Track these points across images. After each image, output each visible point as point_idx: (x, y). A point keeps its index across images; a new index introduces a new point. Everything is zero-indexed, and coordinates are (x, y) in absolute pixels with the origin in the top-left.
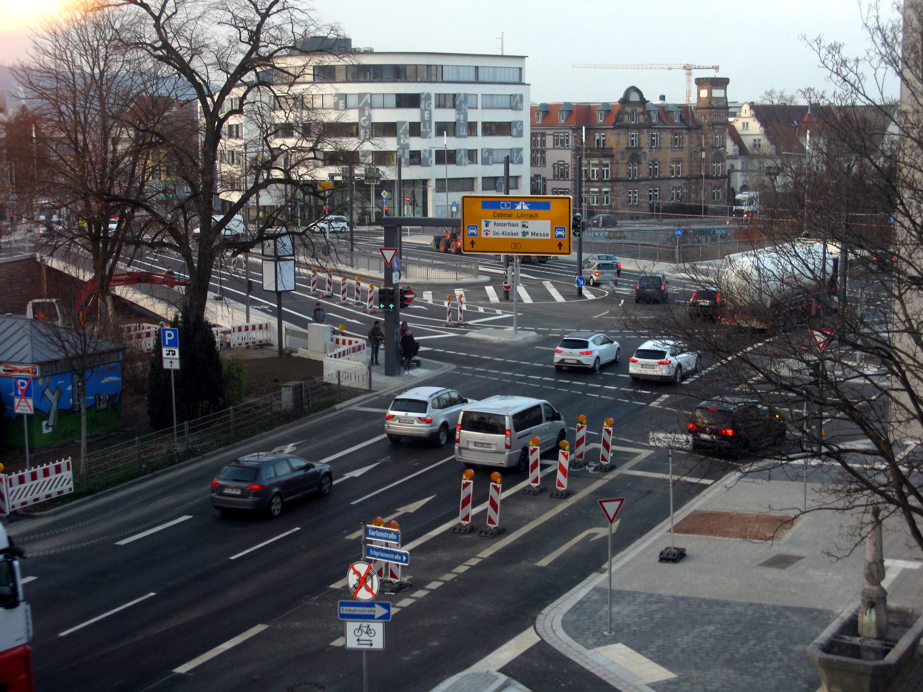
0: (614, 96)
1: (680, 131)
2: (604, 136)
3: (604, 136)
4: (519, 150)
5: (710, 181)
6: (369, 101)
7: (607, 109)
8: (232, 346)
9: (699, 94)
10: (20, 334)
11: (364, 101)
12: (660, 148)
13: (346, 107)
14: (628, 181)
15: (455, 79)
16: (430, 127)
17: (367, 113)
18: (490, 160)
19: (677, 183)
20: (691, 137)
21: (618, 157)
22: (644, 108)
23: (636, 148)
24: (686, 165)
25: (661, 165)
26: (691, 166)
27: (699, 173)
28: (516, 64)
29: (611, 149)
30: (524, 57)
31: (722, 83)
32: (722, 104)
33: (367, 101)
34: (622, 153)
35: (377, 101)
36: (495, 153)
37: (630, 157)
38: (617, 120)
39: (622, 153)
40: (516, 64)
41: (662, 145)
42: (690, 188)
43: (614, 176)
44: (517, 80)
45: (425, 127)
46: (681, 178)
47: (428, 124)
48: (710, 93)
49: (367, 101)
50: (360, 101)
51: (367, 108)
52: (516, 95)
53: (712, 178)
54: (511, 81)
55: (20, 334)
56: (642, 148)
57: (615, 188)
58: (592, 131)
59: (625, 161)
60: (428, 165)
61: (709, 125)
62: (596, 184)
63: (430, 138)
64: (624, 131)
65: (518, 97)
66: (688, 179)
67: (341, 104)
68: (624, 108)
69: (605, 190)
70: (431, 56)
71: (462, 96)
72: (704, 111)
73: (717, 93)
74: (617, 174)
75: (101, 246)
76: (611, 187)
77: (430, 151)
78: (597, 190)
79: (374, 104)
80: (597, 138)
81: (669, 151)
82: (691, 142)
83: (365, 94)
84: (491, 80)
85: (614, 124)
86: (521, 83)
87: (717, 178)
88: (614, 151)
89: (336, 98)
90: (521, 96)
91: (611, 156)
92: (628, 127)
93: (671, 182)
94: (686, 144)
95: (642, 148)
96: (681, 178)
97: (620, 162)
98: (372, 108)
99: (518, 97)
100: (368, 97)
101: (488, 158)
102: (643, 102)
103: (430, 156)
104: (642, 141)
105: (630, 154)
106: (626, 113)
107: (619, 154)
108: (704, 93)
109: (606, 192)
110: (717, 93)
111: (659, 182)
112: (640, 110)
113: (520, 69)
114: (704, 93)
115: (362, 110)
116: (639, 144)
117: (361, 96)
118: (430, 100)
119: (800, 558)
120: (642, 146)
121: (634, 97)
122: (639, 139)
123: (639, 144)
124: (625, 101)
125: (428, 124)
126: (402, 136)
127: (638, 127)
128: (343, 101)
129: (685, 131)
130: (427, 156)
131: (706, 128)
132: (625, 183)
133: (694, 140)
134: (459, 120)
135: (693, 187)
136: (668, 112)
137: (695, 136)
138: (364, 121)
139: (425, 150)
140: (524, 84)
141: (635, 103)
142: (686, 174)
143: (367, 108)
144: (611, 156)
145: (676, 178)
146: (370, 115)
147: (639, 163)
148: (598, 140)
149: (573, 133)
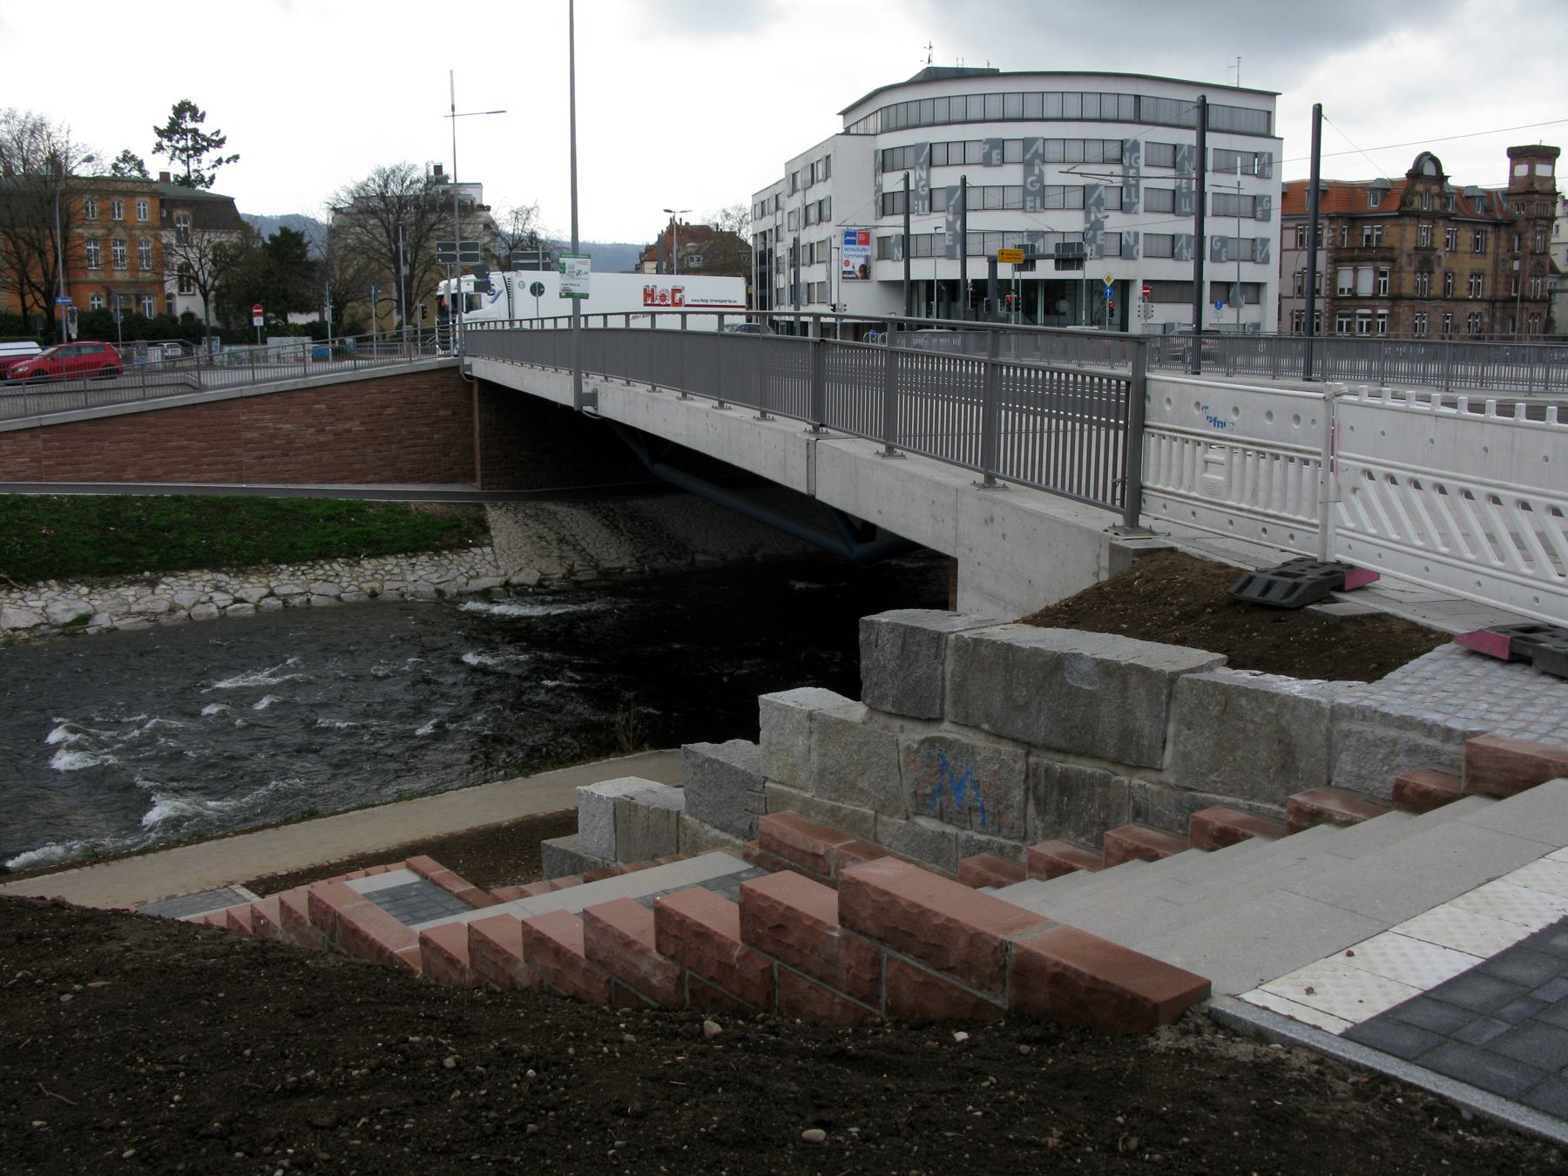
0: (1397, 168)
1: (1484, 228)
2: (1378, 229)
3: (1378, 229)
4: (1265, 242)
5: (1526, 305)
6: (1041, 151)
7: (1383, 189)
8: (172, 179)
9: (1512, 171)
10: (1103, 433)
11: (1032, 151)
12: (1456, 252)
13: (1003, 162)
14: (1415, 298)
15: (1174, 122)
16: (1137, 196)
17: (1037, 171)
18: (1224, 255)
19: (1476, 308)
20: (1498, 239)
21: (1404, 260)
22: (1442, 188)
23: (1426, 249)
24: (1489, 280)
25: (1456, 278)
26: (1495, 282)
27: (1507, 293)
28: (1260, 104)
29: (1392, 249)
30: (1274, 95)
31: (1549, 154)
32: (1547, 187)
33: (1037, 150)
34: (1409, 255)
35: (1054, 151)
36: (1230, 243)
37: (1420, 262)
38: (1403, 203)
39: (1409, 255)
40: (1260, 104)
41: (1459, 248)
42: (1493, 315)
43: (1396, 291)
44: (1263, 130)
45: (1129, 195)
46: (1482, 300)
47: (1133, 189)
48: (1532, 170)
49: (1037, 150)
50: (1025, 151)
51: (1037, 161)
52: (1263, 154)
53: (1530, 301)
54: (1255, 130)
55: (1103, 433)
56: (1436, 249)
57: (1396, 310)
58: (1359, 223)
59: (1412, 269)
60: (1133, 258)
61: (1528, 220)
62: (1366, 303)
63: (1136, 213)
64: (1413, 221)
65: (1265, 158)
66: (1492, 302)
67: (996, 155)
68: (1413, 186)
69: (1381, 311)
70: (1139, 82)
71: (1185, 148)
72: (1520, 197)
73: (1542, 170)
74: (1400, 287)
75: (799, 585)
76: (1390, 308)
77: (1137, 234)
78: (1368, 311)
79: (1049, 157)
80: (1367, 232)
81: (1467, 257)
82: (1497, 246)
83: (1034, 140)
84: (1226, 127)
85: (1398, 210)
86: (1268, 135)
87: (1535, 301)
88: (1397, 252)
89: (987, 147)
90: (1270, 155)
91: (1393, 260)
92: (1418, 216)
93: (1469, 305)
94: (1490, 249)
95: (1436, 249)
96: (1482, 300)
97: (1406, 268)
98: (1044, 162)
99: (1265, 158)
100: (1040, 143)
101: (1220, 251)
102: (1441, 178)
103: (1136, 241)
104: (1436, 238)
105: (1419, 257)
106: (1417, 193)
107: (1405, 256)
108: (1522, 170)
109: (1382, 316)
110: (1542, 170)
111: (1452, 304)
112: (1435, 189)
113: (1269, 113)
114: (1522, 170)
115: (1028, 165)
116: (1432, 242)
117: (1027, 143)
118: (1138, 151)
119: (1025, 621)
120: (1436, 246)
121: (1429, 170)
122: (1432, 235)
123: (1432, 242)
124: (1415, 174)
125: (1133, 189)
126: (1093, 209)
127: (1432, 217)
128: (999, 151)
129: (1490, 229)
130: (1131, 242)
131: (1521, 224)
132: (1411, 303)
133: (1503, 243)
134: (1180, 187)
135: (1498, 315)
136: (1468, 197)
137: (1503, 235)
138: (1032, 183)
139: (1129, 233)
140: (1273, 137)
141: (1430, 178)
142: (1488, 294)
143: (1037, 161)
144: (1393, 260)
145: (1475, 300)
146: (1041, 174)
147: (1431, 272)
148: (1368, 236)
149: (1331, 223)
